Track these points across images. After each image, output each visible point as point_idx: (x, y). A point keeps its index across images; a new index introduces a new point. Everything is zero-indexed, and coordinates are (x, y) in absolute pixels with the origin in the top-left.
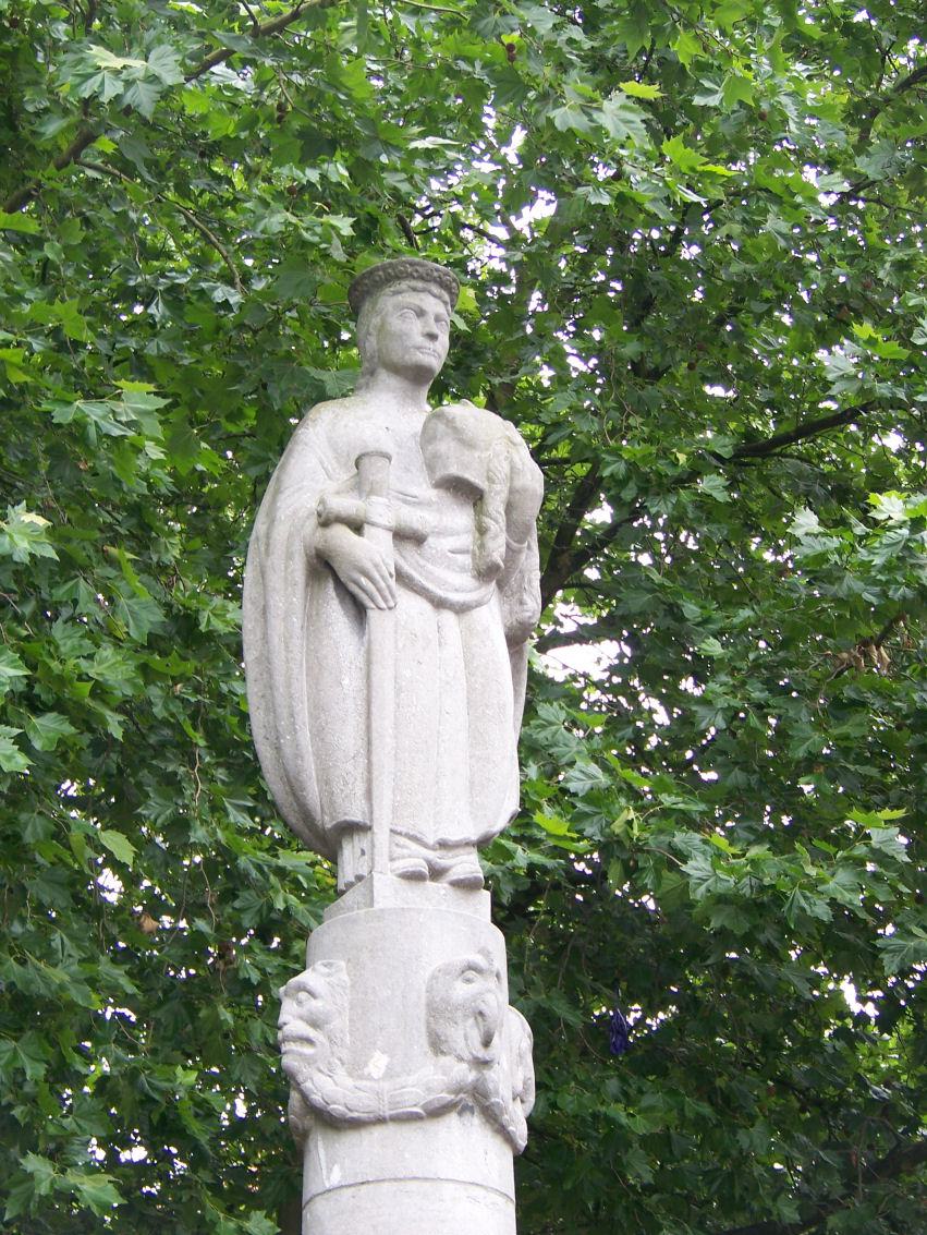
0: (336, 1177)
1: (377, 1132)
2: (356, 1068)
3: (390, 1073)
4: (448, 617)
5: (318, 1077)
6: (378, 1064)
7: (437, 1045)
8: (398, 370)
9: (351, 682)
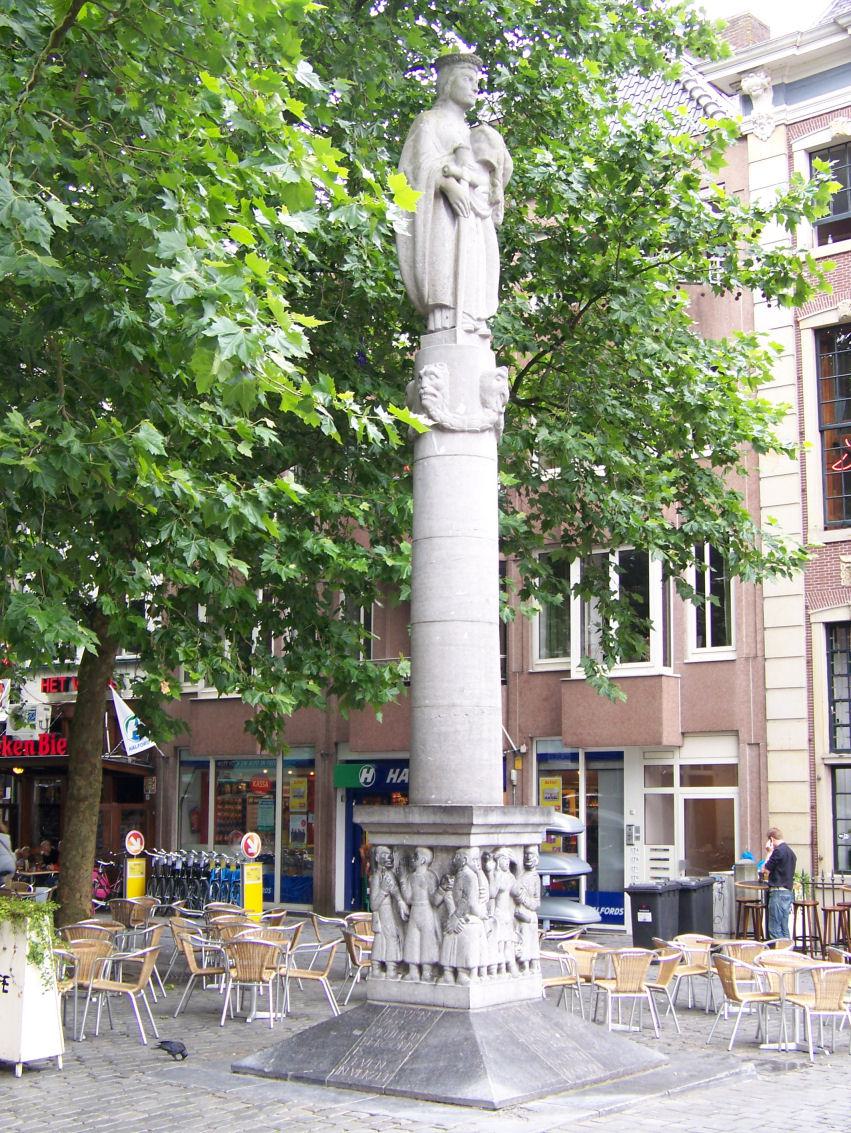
0: (442, 451)
1: (461, 435)
2: (452, 408)
5: (439, 412)
6: (461, 408)
7: (484, 404)
8: (458, 102)
9: (449, 246)
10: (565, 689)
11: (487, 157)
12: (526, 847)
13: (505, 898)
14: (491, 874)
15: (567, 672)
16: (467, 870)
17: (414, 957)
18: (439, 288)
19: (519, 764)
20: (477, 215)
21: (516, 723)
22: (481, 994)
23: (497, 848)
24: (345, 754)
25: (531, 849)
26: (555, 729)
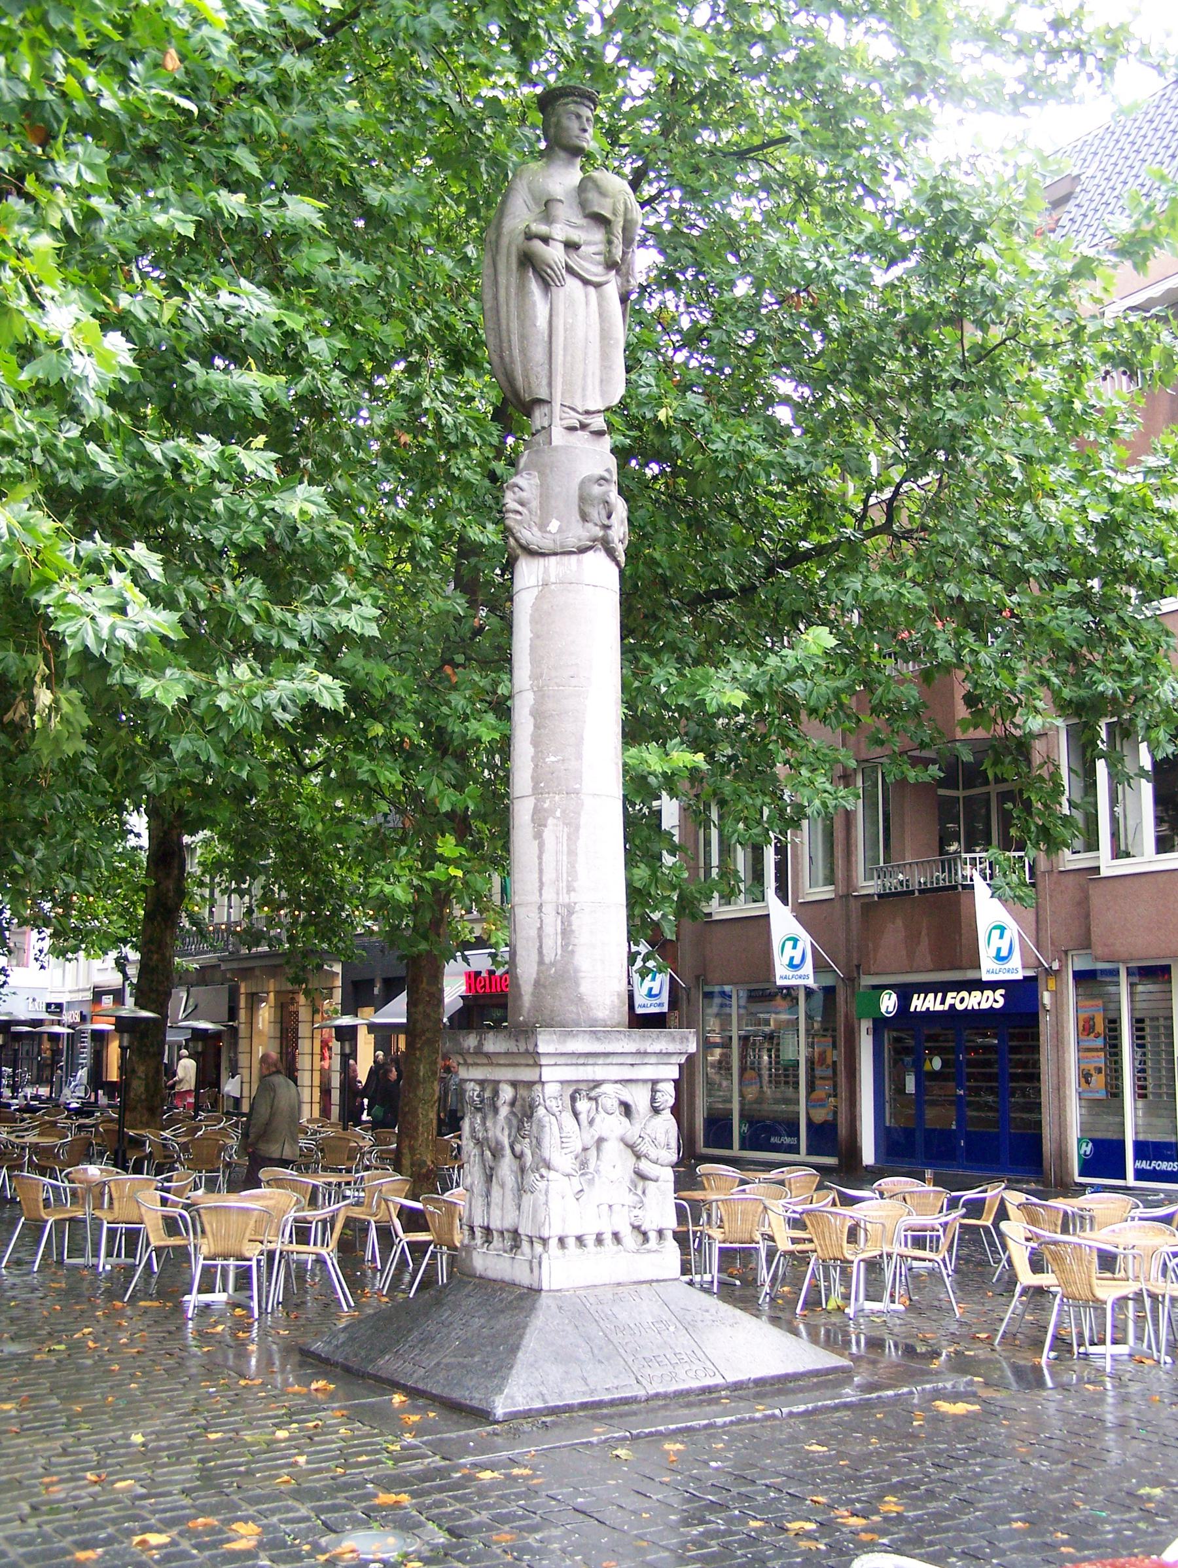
2: (543, 527)
3: (560, 530)
4: (591, 289)
6: (554, 526)
7: (584, 517)
10: (1095, 893)
11: (596, 209)
12: (655, 1082)
13: (613, 1148)
14: (583, 1118)
15: (1097, 869)
16: (541, 1111)
17: (495, 1224)
18: (533, 379)
19: (1052, 985)
20: (586, 282)
21: (1049, 931)
22: (560, 1272)
23: (598, 1084)
24: (867, 981)
25: (660, 1086)
26: (1085, 944)
